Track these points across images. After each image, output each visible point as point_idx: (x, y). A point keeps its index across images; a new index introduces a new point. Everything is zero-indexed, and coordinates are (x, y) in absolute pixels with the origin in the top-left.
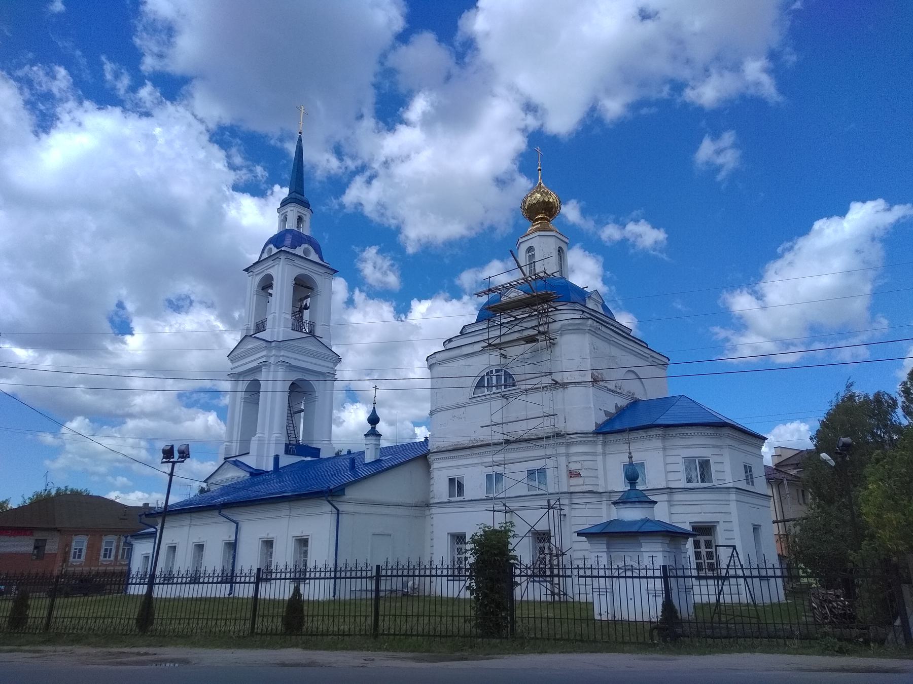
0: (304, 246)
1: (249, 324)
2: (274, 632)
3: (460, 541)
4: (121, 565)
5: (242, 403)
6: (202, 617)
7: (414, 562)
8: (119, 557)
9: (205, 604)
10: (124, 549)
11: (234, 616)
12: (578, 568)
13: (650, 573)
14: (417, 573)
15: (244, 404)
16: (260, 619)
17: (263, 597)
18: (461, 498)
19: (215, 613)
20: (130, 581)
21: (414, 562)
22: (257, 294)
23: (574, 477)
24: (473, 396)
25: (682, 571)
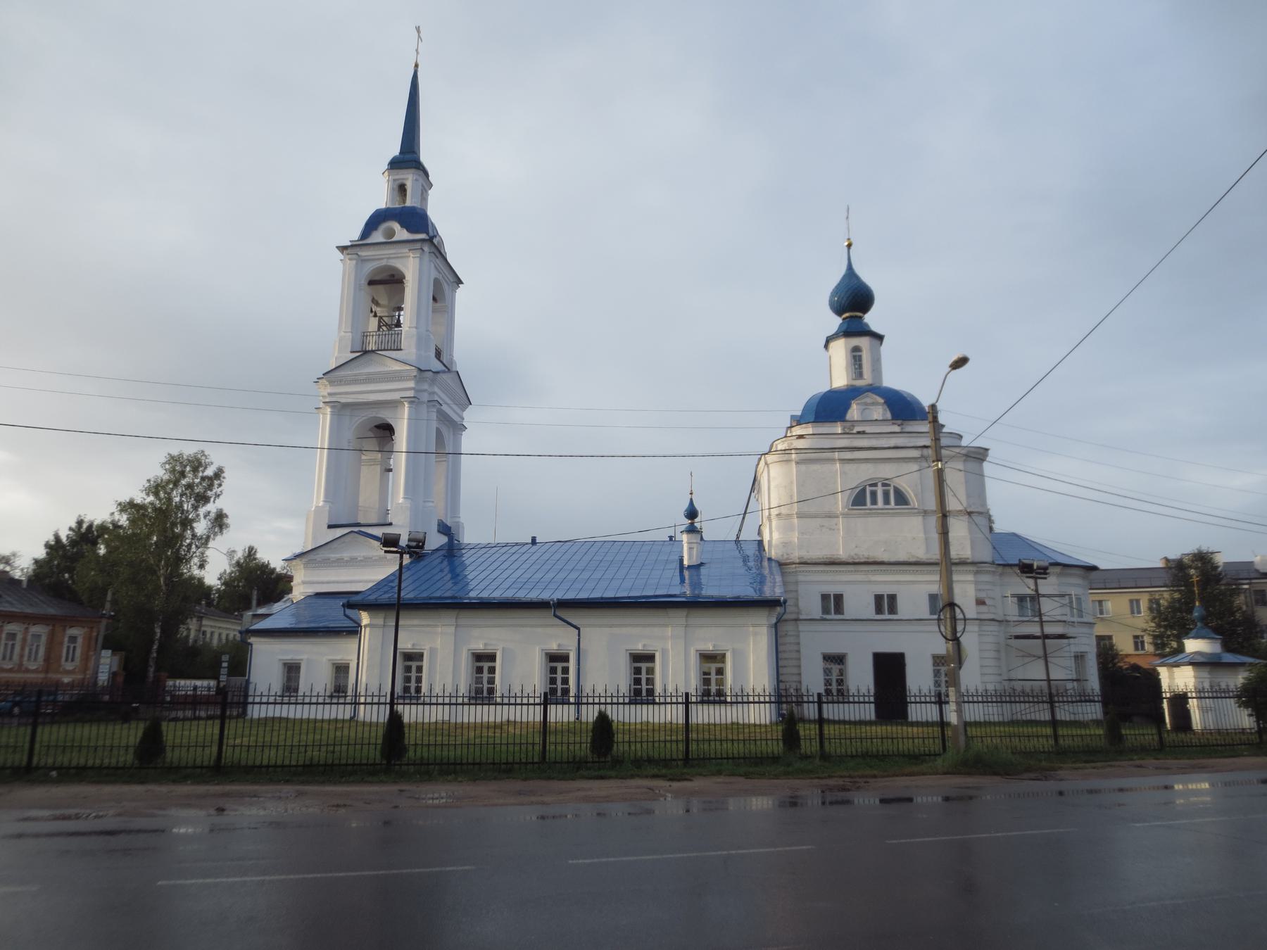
2: (464, 761)
4: (28, 671)
6: (343, 747)
8: (26, 658)
9: (197, 736)
10: (68, 647)
12: (759, 695)
13: (440, 700)
19: (669, 733)
20: (250, 699)
25: (530, 699)
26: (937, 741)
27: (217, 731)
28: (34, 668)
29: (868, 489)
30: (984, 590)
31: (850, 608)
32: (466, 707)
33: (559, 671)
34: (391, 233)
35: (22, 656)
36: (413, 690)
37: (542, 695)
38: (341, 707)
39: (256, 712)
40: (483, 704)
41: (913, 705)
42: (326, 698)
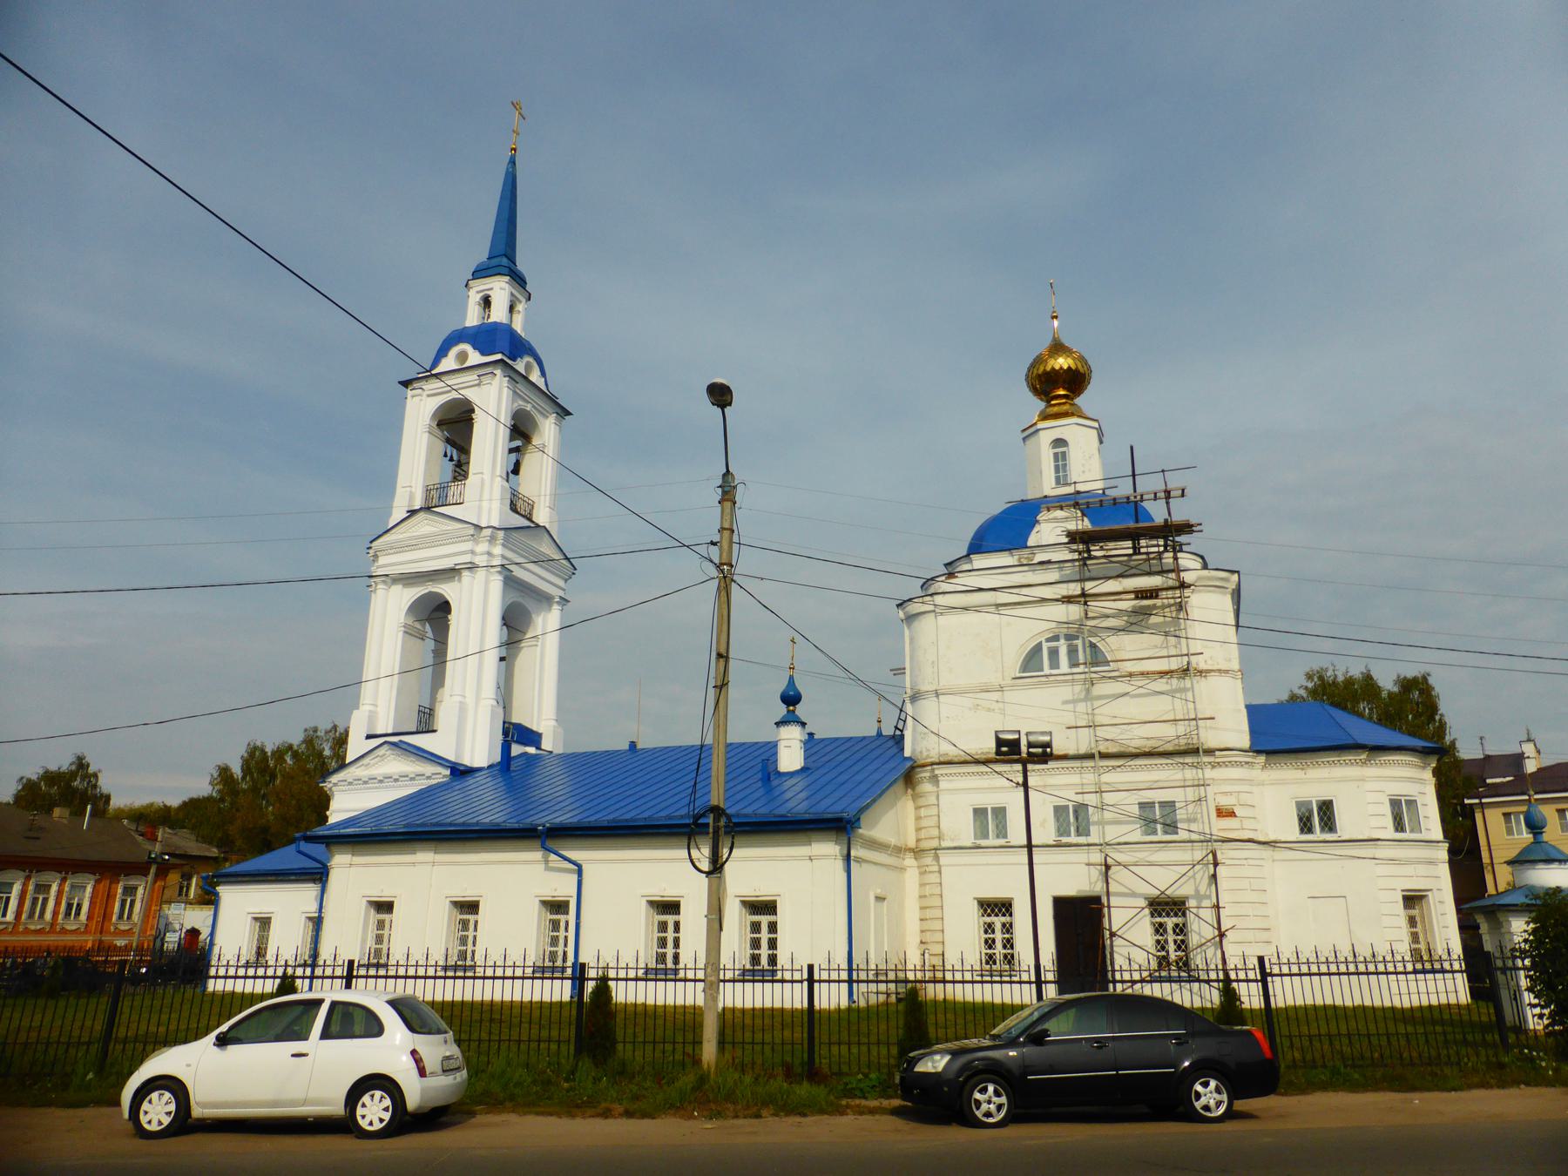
0: (528, 359)
1: (413, 485)
3: (985, 911)
4: (64, 931)
5: (401, 634)
7: (1345, 952)
8: (24, 917)
10: (35, 900)
11: (475, 1036)
14: (1447, 966)
15: (404, 637)
16: (119, 1047)
17: (1281, 1004)
18: (1002, 842)
20: (212, 972)
21: (1345, 952)
22: (429, 432)
23: (1224, 816)
24: (1018, 675)
25: (517, 969)
26: (564, 1048)
27: (101, 1019)
28: (74, 928)
29: (1045, 646)
30: (1231, 793)
31: (1346, 824)
32: (528, 982)
33: (764, 928)
34: (463, 356)
35: (55, 913)
36: (764, 961)
37: (346, 964)
38: (469, 982)
39: (212, 986)
40: (763, 981)
41: (825, 986)
42: (439, 969)
